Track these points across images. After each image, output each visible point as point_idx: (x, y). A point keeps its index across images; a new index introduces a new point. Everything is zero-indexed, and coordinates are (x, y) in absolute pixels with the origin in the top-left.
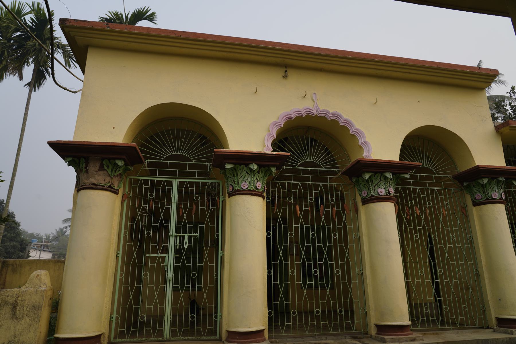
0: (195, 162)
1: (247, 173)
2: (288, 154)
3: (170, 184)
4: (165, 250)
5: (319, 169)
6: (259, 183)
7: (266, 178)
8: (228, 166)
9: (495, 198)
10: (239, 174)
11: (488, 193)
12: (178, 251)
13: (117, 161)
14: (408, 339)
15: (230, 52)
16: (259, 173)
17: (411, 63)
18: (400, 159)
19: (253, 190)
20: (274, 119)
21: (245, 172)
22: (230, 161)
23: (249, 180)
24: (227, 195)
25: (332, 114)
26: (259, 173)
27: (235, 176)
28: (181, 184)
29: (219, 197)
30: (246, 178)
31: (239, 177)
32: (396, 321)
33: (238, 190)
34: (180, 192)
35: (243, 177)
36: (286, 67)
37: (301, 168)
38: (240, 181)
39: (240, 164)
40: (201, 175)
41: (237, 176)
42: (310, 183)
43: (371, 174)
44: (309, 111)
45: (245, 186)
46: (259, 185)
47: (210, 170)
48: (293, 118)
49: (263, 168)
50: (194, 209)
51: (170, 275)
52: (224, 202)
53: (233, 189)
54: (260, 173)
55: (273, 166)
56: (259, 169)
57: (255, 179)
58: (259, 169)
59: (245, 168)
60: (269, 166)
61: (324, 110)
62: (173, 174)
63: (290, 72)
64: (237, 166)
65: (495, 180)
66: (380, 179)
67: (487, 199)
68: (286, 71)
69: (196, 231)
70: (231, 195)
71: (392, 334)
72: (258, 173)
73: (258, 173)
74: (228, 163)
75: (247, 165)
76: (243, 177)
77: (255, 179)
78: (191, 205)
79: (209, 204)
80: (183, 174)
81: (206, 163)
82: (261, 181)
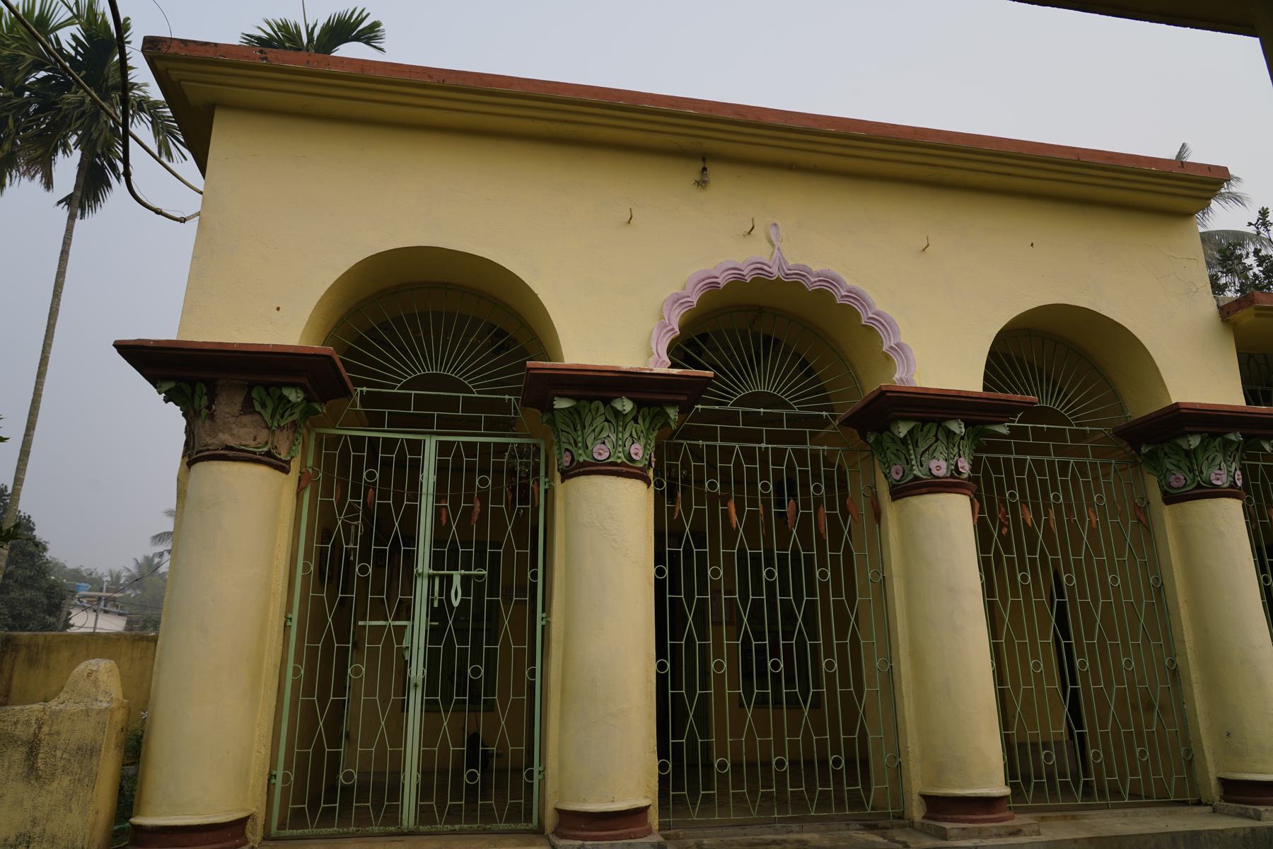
0: (1077, 425)
1: (607, 420)
2: (709, 374)
3: (417, 447)
4: (405, 611)
5: (784, 412)
7: (655, 434)
8: (561, 404)
9: (1219, 483)
11: (1201, 472)
12: (437, 614)
14: (1002, 832)
15: (566, 121)
16: (636, 422)
17: (1013, 150)
19: (623, 464)
20: (676, 289)
21: (603, 418)
22: (566, 392)
24: (558, 475)
25: (818, 275)
26: (636, 422)
27: (579, 427)
28: (443, 448)
29: (538, 481)
30: (604, 434)
32: (973, 786)
33: (586, 464)
34: (441, 468)
35: (597, 431)
36: (704, 160)
37: (741, 409)
38: (589, 441)
39: (591, 400)
42: (763, 445)
43: (911, 425)
44: (759, 267)
45: (601, 452)
49: (646, 409)
50: (477, 510)
51: (417, 672)
52: (550, 493)
53: (572, 460)
54: (640, 421)
55: (673, 404)
56: (638, 412)
57: (627, 435)
58: (638, 412)
59: (602, 410)
60: (661, 404)
61: (797, 267)
62: (423, 423)
63: (717, 173)
64: (584, 402)
65: (1219, 439)
66: (936, 436)
67: (1199, 486)
68: (705, 169)
69: (481, 565)
71: (974, 817)
72: (635, 420)
73: (635, 420)
74: (561, 396)
75: (607, 402)
76: (597, 431)
77: (627, 435)
78: (469, 499)
79: (514, 497)
80: (448, 424)
82: (643, 441)
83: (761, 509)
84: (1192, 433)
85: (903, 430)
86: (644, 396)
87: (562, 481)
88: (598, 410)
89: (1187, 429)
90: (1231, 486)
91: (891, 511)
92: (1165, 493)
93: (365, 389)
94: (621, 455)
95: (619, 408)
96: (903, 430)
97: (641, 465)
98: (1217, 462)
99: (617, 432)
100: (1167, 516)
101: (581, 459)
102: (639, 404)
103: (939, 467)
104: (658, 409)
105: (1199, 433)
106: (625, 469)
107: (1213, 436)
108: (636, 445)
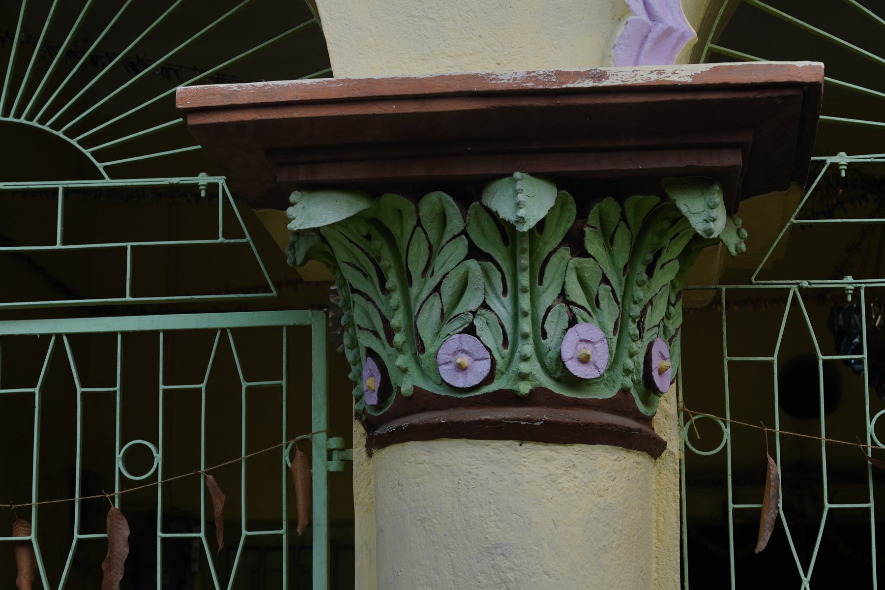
0: (114, 172)
1: (474, 253)
2: (808, 69)
6: (581, 330)
7: (665, 276)
8: (314, 213)
10: (416, 270)
16: (580, 251)
19: (539, 397)
21: (460, 248)
22: (326, 174)
23: (502, 308)
24: (358, 430)
26: (580, 251)
27: (392, 281)
29: (306, 447)
30: (471, 302)
31: (420, 289)
33: (420, 401)
35: (448, 289)
39: (415, 191)
40: (164, 280)
41: (407, 279)
45: (462, 362)
46: (586, 347)
47: (232, 229)
48: (224, 177)
49: (610, 206)
50: (121, 550)
52: (341, 485)
53: (386, 388)
54: (593, 244)
55: (700, 181)
56: (582, 215)
57: (548, 296)
58: (582, 215)
59: (456, 223)
60: (660, 186)
64: (392, 200)
72: (575, 243)
73: (575, 243)
74: (313, 187)
75: (469, 193)
76: (448, 289)
77: (548, 296)
78: (95, 517)
79: (233, 503)
81: (203, 179)
82: (609, 312)
86: (607, 165)
87: (370, 455)
88: (443, 219)
93: (843, 159)
94: (533, 367)
95: (506, 212)
97: (607, 393)
99: (510, 289)
101: (406, 387)
102: (580, 192)
104: (652, 200)
106: (541, 414)
108: (585, 329)
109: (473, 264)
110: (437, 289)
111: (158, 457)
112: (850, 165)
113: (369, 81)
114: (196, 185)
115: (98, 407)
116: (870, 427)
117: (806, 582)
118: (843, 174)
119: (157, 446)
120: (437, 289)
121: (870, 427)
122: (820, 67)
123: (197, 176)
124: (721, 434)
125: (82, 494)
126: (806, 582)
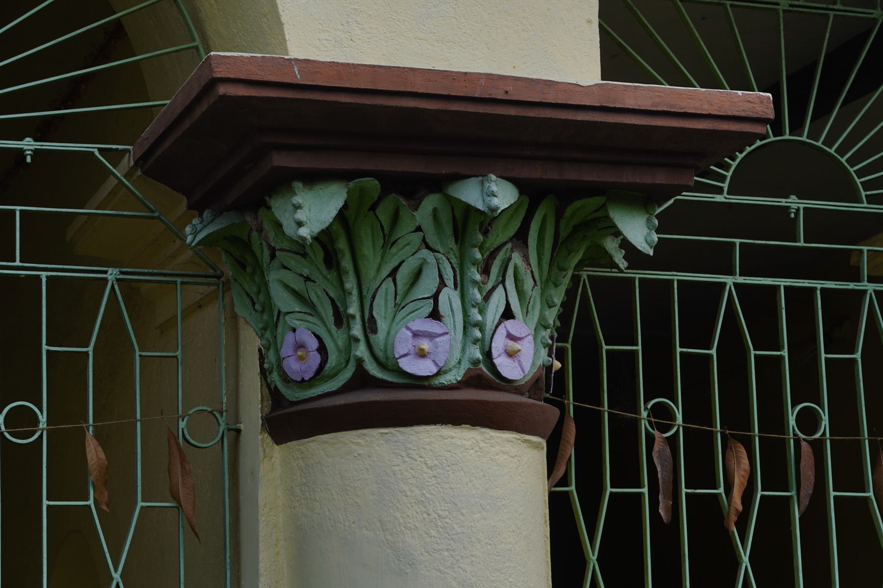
0: (871, 199)
9: (424, 368)
11: (370, 326)
13: (470, 193)
18: (614, 64)
27: (347, 263)
35: (403, 275)
38: (381, 311)
65: (431, 202)
67: (361, 380)
70: (292, 421)
73: (521, 238)
83: (645, 490)
84: (313, 178)
85: (313, 211)
89: (282, 160)
90: (473, 380)
91: (271, 468)
92: (275, 397)
96: (313, 211)
98: (428, 284)
100: (271, 468)
102: (532, 193)
103: (429, 349)
105: (344, 176)
107: (412, 188)
109: (425, 253)
110: (393, 274)
111: (43, 418)
112: (36, 152)
113: (550, 84)
114: (21, 152)
115: (769, 369)
116: (792, 421)
117: (117, 576)
118: (29, 159)
119: (822, 406)
120: (393, 274)
121: (792, 421)
122: (769, 98)
123: (22, 140)
124: (36, 422)
125: (859, 444)
126: (117, 576)
